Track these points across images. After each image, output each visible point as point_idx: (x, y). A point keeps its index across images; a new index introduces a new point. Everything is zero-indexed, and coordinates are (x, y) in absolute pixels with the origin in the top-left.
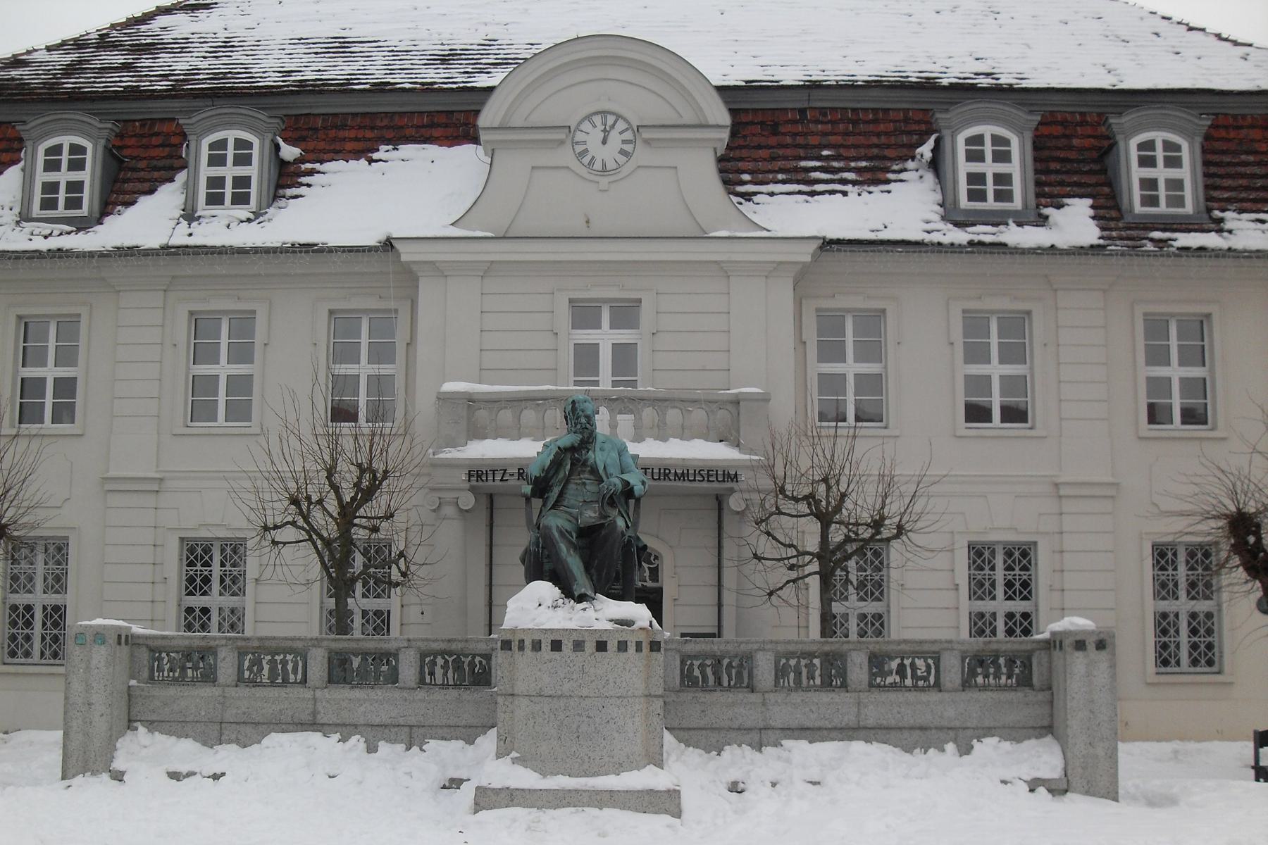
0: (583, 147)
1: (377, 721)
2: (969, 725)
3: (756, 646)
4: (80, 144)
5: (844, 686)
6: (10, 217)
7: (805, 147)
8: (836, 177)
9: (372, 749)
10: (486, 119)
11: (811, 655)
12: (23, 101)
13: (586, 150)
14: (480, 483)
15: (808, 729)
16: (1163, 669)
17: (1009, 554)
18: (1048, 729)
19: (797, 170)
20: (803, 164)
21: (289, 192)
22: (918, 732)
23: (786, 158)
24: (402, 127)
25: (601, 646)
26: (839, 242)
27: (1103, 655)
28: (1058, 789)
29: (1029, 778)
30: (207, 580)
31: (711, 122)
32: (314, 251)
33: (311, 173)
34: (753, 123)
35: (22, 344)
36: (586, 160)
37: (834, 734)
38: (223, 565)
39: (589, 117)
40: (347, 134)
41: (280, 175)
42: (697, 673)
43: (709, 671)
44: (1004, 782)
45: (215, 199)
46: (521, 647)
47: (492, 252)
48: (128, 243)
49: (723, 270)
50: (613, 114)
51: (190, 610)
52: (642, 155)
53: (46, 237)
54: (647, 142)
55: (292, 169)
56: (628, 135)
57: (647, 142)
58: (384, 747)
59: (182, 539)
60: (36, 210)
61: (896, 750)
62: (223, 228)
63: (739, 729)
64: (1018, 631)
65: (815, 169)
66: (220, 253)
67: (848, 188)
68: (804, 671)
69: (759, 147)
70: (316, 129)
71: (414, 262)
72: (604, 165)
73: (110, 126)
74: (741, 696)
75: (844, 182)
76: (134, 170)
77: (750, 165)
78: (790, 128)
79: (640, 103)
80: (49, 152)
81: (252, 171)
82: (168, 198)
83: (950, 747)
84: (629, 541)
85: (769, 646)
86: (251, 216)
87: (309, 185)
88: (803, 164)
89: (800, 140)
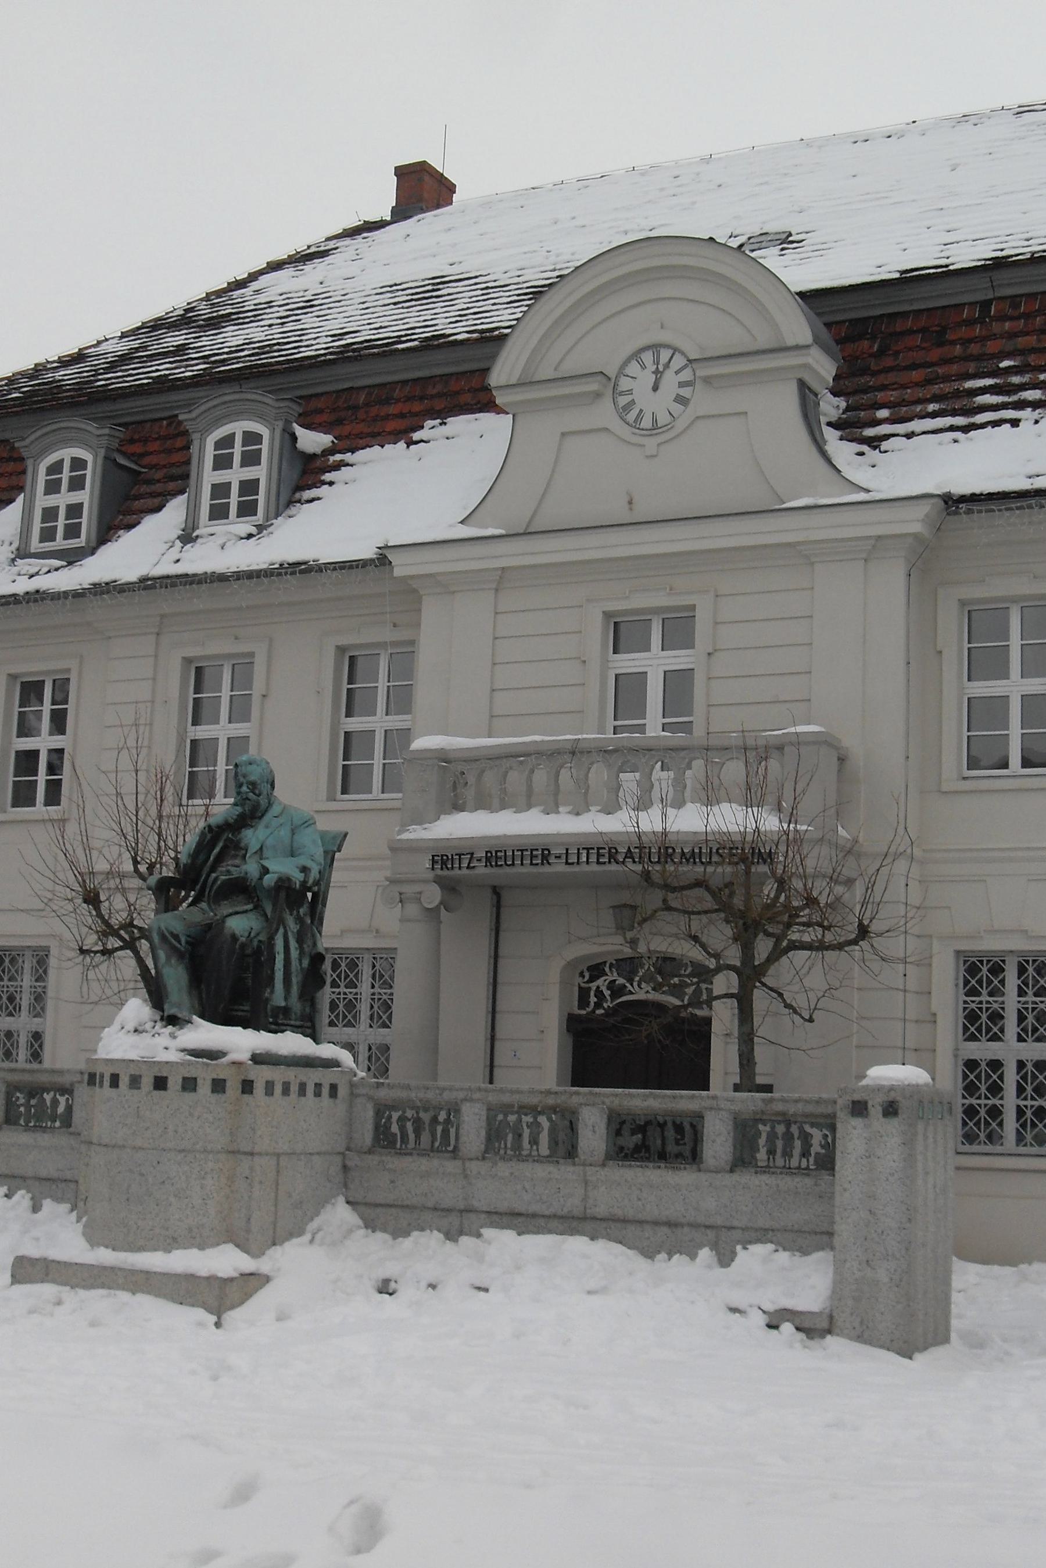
0: (629, 398)
1: (44, 1174)
2: (736, 1223)
3: (461, 1095)
4: (71, 460)
5: (571, 1153)
6: (5, 552)
7: (979, 358)
8: (1014, 398)
9: (36, 1208)
10: (503, 372)
11: (535, 1111)
12: (42, 409)
13: (633, 402)
14: (445, 873)
15: (520, 1214)
16: (967, 1148)
17: (1022, 970)
18: (808, 1237)
19: (958, 394)
20: (970, 384)
21: (307, 494)
22: (665, 1230)
23: (946, 379)
24: (457, 393)
25: (160, 1083)
26: (974, 498)
27: (893, 1126)
28: (813, 1328)
29: (770, 1307)
30: (996, 1017)
31: (790, 342)
32: (302, 572)
33: (338, 466)
34: (911, 332)
35: (345, 686)
36: (631, 416)
37: (554, 1224)
38: (1021, 993)
39: (636, 355)
40: (392, 410)
41: (304, 472)
42: (395, 1128)
43: (409, 1126)
44: (734, 1310)
45: (219, 513)
46: (160, 1083)
47: (510, 553)
48: (292, 558)
49: (802, 555)
50: (667, 346)
51: (971, 1065)
52: (703, 401)
53: (31, 576)
54: (707, 380)
55: (318, 463)
56: (686, 375)
57: (707, 380)
58: (48, 1204)
59: (958, 953)
60: (35, 545)
61: (630, 1252)
62: (227, 550)
63: (435, 1209)
64: (983, 1089)
65: (983, 390)
66: (200, 582)
67: (1026, 414)
68: (526, 1133)
69: (914, 366)
70: (355, 408)
71: (412, 577)
72: (655, 421)
73: (106, 431)
74: (436, 1162)
75: (1020, 405)
76: (149, 482)
77: (893, 395)
78: (963, 332)
79: (699, 324)
80: (218, 445)
81: (260, 472)
82: (172, 515)
83: (705, 1254)
84: (259, 947)
85: (477, 1095)
86: (254, 530)
87: (331, 483)
88: (970, 384)
89: (974, 349)
